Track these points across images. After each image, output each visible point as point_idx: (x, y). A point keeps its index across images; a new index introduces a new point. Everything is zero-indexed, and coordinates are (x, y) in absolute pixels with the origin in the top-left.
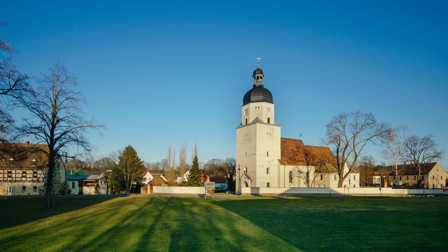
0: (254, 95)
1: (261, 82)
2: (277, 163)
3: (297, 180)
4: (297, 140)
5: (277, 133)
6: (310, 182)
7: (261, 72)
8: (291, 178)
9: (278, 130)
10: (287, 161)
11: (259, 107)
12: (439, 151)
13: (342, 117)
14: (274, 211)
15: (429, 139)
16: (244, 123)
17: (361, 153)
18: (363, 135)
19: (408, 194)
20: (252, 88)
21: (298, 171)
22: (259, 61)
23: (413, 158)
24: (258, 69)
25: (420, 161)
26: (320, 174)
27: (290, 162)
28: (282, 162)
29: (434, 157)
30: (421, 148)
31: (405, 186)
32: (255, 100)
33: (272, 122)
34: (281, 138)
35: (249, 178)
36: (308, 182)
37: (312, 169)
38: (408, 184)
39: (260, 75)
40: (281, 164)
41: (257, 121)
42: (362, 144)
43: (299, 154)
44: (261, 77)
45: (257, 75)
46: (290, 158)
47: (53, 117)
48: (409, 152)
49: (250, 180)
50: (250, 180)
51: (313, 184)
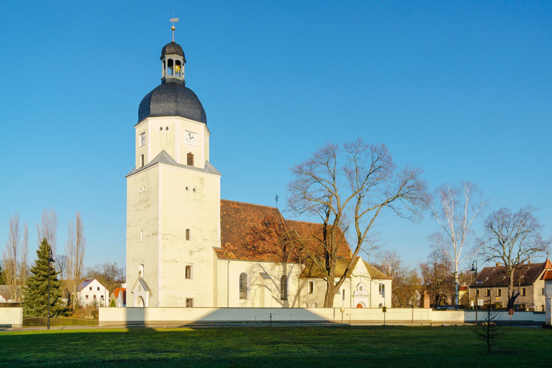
0: (158, 101)
1: (180, 73)
2: (212, 254)
3: (258, 294)
4: (268, 209)
5: (211, 191)
6: (291, 299)
7: (178, 50)
8: (243, 288)
9: (213, 182)
10: (234, 252)
11: (167, 128)
12: (545, 239)
13: (330, 152)
15: (527, 214)
17: (369, 232)
18: (374, 195)
19: (465, 322)
20: (160, 83)
21: (261, 274)
22: (174, 28)
23: (502, 252)
24: (173, 44)
25: (514, 257)
26: (310, 280)
27: (243, 255)
28: (221, 254)
29: (535, 250)
30: (514, 233)
31: (465, 307)
32: (160, 111)
33: (200, 161)
35: (147, 288)
36: (284, 298)
37: (294, 269)
38: (499, 303)
39: (175, 58)
40: (219, 258)
41: (163, 158)
42: (372, 213)
43: (267, 238)
44: (178, 63)
45: (168, 57)
46: (245, 246)
48: (495, 241)
49: (148, 293)
50: (148, 293)
51: (297, 302)
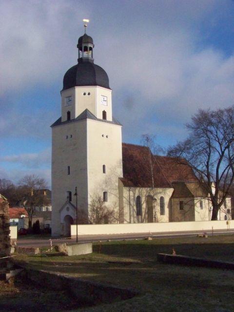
9: (118, 129)
11: (89, 94)
14: (73, 262)
16: (65, 119)
20: (76, 63)
33: (109, 117)
34: (124, 144)
47: (17, 268)
